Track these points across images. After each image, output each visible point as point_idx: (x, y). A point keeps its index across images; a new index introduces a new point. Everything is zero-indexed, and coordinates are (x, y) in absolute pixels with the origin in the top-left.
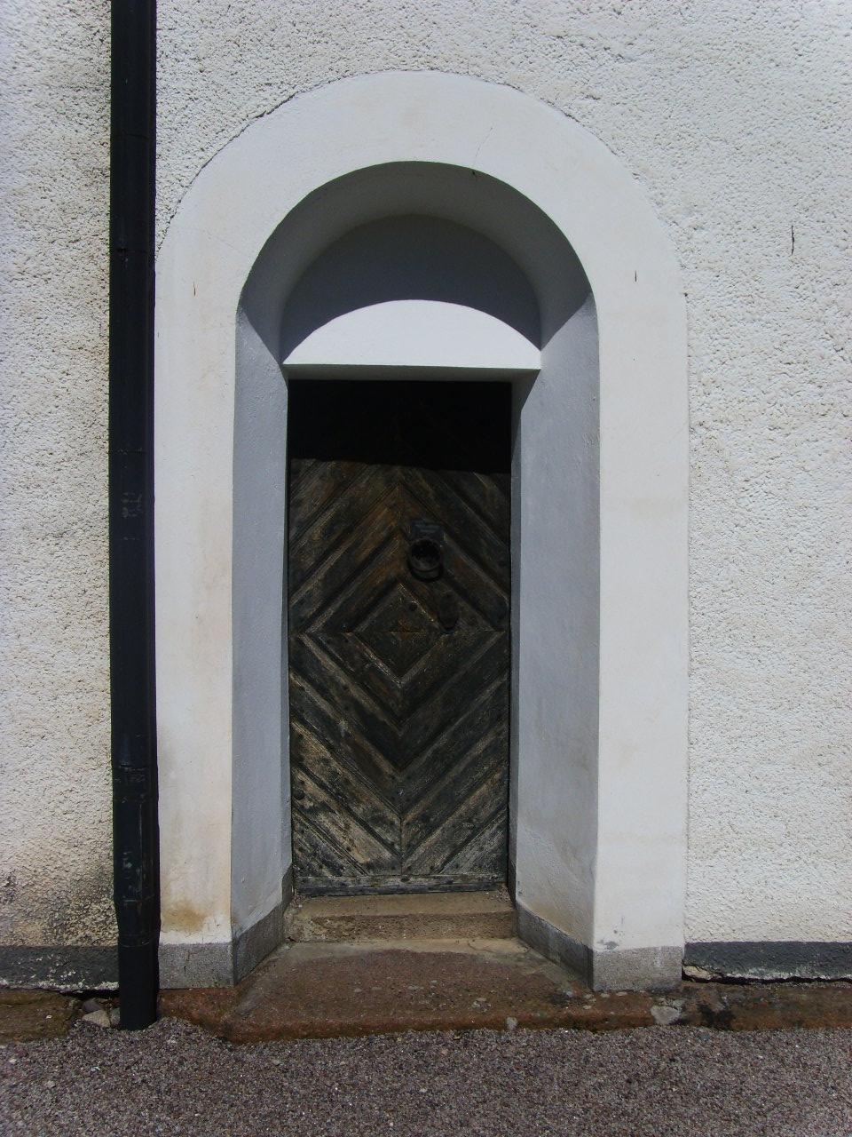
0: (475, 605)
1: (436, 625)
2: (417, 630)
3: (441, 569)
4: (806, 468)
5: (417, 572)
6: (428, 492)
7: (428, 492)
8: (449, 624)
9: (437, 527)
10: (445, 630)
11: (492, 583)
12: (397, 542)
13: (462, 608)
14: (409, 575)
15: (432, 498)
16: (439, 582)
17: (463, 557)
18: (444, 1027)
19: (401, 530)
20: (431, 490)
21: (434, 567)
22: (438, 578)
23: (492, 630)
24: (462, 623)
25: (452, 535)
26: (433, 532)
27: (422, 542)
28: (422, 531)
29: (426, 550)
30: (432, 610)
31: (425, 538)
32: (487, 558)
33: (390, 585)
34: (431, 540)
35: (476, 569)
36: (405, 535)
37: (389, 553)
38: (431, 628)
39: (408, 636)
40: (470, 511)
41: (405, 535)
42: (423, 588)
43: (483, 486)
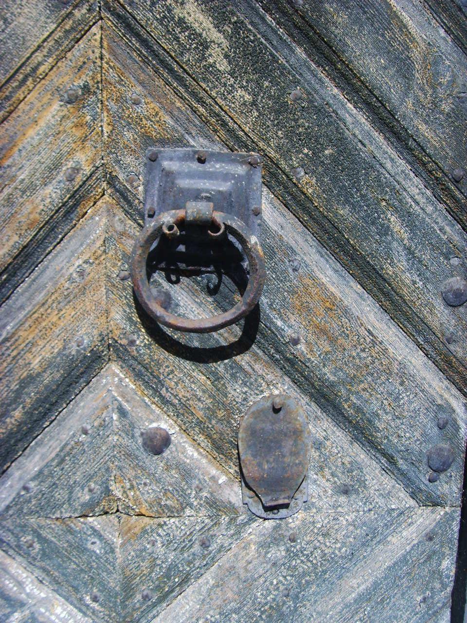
0: (361, 431)
1: (235, 494)
2: (172, 512)
3: (252, 324)
4: (53, 291)
5: (169, 331)
6: (205, 45)
7: (205, 45)
8: (274, 491)
9: (241, 170)
10: (261, 512)
11: (417, 362)
12: (100, 221)
13: (319, 445)
14: (142, 338)
15: (223, 66)
16: (243, 360)
17: (328, 275)
18: (334, 51)
19: (112, 181)
20: (215, 35)
21: (229, 316)
22: (241, 346)
23: (412, 502)
24: (317, 488)
25: (295, 201)
26: (225, 187)
27: (182, 223)
28: (184, 183)
29: (200, 250)
30: (222, 447)
31: (195, 210)
32: (407, 277)
33: (80, 371)
34: (218, 217)
35: (368, 313)
36: (124, 196)
37: (66, 262)
38: (216, 506)
39: (144, 531)
40: (355, 120)
41: (124, 196)
42: (188, 379)
43: (403, 27)
